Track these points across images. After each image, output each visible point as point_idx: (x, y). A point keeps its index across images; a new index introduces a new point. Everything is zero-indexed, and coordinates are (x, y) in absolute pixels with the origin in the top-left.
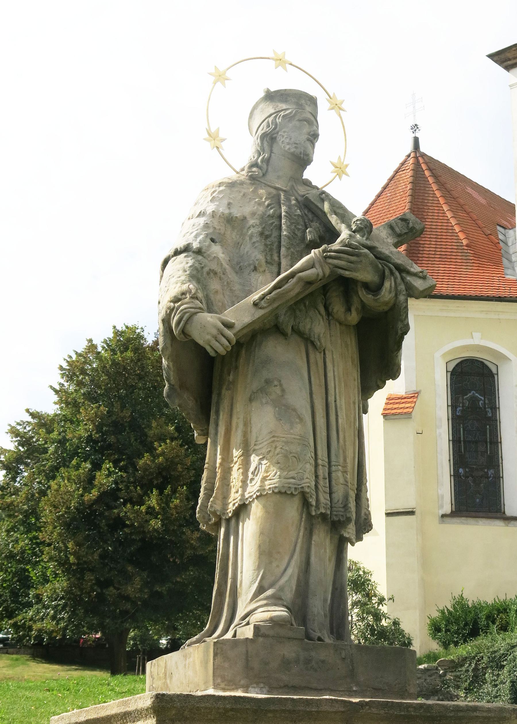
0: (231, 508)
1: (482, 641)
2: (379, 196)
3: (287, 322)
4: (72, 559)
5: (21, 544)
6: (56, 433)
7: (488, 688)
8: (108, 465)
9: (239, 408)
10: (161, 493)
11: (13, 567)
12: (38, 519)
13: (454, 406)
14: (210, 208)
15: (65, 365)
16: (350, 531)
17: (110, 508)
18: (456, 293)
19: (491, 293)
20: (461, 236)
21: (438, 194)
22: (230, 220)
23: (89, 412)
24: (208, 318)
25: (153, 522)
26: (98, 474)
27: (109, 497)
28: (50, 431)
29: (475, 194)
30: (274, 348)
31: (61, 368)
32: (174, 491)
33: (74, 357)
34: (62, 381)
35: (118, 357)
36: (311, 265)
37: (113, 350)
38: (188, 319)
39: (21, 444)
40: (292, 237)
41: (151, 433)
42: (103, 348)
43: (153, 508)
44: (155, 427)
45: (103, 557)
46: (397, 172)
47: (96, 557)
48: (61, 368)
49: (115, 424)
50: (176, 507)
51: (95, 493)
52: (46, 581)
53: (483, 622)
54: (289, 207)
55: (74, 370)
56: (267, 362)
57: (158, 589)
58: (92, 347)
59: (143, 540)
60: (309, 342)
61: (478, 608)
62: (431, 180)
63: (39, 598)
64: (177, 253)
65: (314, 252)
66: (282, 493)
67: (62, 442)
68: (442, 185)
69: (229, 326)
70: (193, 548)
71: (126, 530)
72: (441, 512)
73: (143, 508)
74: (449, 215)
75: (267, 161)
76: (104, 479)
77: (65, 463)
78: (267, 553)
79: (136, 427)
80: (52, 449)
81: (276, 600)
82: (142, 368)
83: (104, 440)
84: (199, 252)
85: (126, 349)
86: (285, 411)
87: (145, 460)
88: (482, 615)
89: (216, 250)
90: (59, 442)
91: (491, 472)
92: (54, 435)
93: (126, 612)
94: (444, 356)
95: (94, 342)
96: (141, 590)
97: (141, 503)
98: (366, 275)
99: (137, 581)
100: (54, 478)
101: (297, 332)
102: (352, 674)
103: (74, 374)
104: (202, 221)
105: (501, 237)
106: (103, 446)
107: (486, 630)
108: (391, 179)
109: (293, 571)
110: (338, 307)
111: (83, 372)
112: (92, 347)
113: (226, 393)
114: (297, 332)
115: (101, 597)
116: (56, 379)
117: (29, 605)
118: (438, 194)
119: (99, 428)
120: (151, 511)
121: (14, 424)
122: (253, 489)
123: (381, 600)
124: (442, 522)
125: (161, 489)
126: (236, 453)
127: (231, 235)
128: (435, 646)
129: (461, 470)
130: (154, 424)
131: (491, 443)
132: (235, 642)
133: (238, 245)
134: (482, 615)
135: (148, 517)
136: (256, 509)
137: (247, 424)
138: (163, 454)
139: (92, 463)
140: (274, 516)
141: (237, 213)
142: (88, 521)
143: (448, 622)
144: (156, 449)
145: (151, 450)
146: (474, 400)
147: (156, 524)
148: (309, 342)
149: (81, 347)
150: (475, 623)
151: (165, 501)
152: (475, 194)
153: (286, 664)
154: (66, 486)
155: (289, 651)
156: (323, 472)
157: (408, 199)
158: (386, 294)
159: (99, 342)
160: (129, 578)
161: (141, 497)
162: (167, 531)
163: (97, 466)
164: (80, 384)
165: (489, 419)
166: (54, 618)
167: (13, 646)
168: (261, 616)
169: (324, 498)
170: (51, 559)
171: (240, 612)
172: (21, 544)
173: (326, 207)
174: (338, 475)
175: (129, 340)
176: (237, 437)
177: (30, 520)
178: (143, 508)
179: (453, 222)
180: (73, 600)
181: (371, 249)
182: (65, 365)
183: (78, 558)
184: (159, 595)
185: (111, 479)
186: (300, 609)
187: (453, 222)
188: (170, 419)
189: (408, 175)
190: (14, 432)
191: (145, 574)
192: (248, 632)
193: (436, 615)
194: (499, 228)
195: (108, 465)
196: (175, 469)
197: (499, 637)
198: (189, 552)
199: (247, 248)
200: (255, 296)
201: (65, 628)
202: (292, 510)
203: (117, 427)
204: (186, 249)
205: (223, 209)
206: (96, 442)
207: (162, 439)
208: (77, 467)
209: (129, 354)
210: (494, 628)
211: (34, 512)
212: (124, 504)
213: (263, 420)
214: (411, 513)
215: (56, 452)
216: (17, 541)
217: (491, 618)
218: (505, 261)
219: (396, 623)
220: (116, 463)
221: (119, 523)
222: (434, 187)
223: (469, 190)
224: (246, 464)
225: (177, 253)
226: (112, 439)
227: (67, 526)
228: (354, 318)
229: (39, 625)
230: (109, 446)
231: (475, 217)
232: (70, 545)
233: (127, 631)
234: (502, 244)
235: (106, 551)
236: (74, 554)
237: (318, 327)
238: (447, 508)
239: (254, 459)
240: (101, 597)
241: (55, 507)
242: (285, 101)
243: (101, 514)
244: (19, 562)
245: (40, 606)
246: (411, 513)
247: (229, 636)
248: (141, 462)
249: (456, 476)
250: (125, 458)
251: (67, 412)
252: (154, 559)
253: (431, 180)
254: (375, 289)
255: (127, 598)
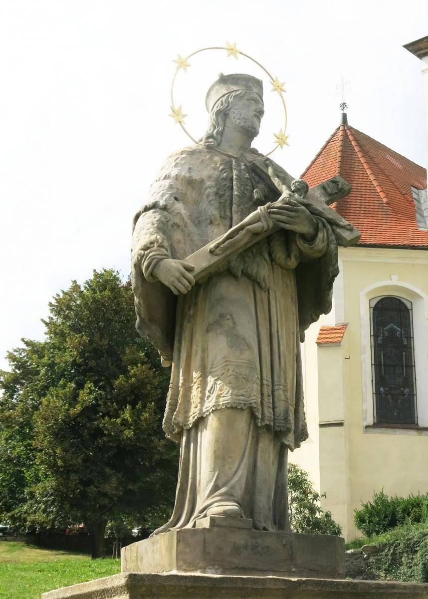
0: (191, 420)
1: (399, 530)
2: (314, 162)
3: (235, 264)
4: (60, 462)
5: (18, 450)
6: (46, 358)
7: (403, 569)
8: (89, 385)
9: (198, 337)
10: (133, 408)
11: (11, 469)
12: (31, 429)
13: (376, 335)
14: (174, 172)
15: (54, 302)
16: (290, 439)
17: (91, 420)
18: (377, 242)
19: (406, 243)
20: (382, 195)
21: (362, 160)
22: (190, 182)
23: (74, 340)
24: (173, 263)
25: (126, 432)
26: (81, 392)
27: (90, 411)
28: (41, 357)
29: (393, 161)
30: (231, 292)
31: (51, 305)
32: (144, 406)
33: (61, 295)
34: (51, 315)
35: (98, 295)
36: (257, 219)
37: (94, 290)
38: (155, 264)
39: (18, 367)
40: (242, 196)
41: (125, 358)
42: (86, 288)
43: (127, 420)
44: (128, 353)
45: (85, 460)
46: (328, 142)
47: (80, 461)
48: (51, 305)
49: (95, 351)
50: (146, 419)
51: (78, 408)
52: (38, 480)
53: (400, 515)
54: (240, 171)
55: (62, 306)
56: (221, 299)
57: (130, 487)
58: (76, 287)
59: (118, 447)
60: (256, 283)
61: (396, 503)
62: (357, 149)
63: (32, 495)
64: (146, 209)
65: (260, 209)
66: (233, 408)
67: (51, 366)
68: (365, 153)
69: (189, 269)
70: (160, 453)
71: (105, 439)
72: (365, 424)
73: (119, 421)
74: (372, 177)
75: (221, 133)
76: (87, 396)
77: (54, 383)
78: (221, 457)
79: (113, 353)
80: (43, 372)
81: (228, 496)
82: (118, 304)
83: (86, 364)
84: (165, 208)
85: (105, 289)
86: (236, 341)
87: (120, 381)
88: (399, 509)
89: (179, 207)
90: (49, 365)
91: (406, 391)
92: (45, 360)
93: (104, 506)
94: (367, 294)
95: (78, 283)
96: (117, 488)
97: (117, 416)
98: (303, 228)
99: (114, 481)
100: (44, 395)
101: (246, 275)
102: (291, 558)
103: (61, 309)
104: (167, 183)
105: (415, 196)
106: (82, 371)
107: (402, 521)
108: (324, 148)
109: (243, 472)
110: (280, 255)
111: (69, 308)
112: (76, 287)
113: (187, 325)
114: (246, 275)
115: (84, 495)
116: (47, 314)
117: (24, 501)
118: (362, 160)
119: (82, 354)
120: (125, 423)
121: (11, 351)
122: (209, 404)
123: (316, 497)
124: (366, 432)
125: (133, 404)
126: (196, 375)
127: (192, 195)
128: (360, 535)
129: (382, 389)
130: (127, 351)
131: (406, 366)
132: (194, 531)
133: (197, 203)
134: (399, 509)
135: (122, 428)
136: (212, 422)
137: (204, 350)
138: (135, 375)
139: (76, 383)
140: (227, 427)
141: (196, 176)
142: (70, 431)
143: (371, 515)
144: (129, 372)
145: (125, 372)
146: (392, 331)
147: (129, 433)
148: (256, 283)
149: (67, 287)
150: (394, 515)
151: (137, 415)
152: (393, 161)
153: (236, 549)
154: (54, 401)
155: (239, 538)
156: (267, 390)
157: (338, 165)
158: (320, 243)
159: (82, 283)
160: (107, 478)
161: (117, 411)
162: (138, 440)
163: (80, 386)
164: (66, 318)
165: (405, 346)
166: (44, 511)
167: (10, 534)
168: (216, 509)
169: (268, 412)
170: (42, 462)
171: (199, 507)
172: (18, 450)
173: (270, 171)
174: (280, 393)
175: (106, 281)
176: (196, 362)
177: (24, 430)
178: (119, 421)
179: (375, 183)
180: (61, 496)
181: (307, 206)
182: (54, 302)
183: (65, 462)
184: (132, 492)
185: (92, 397)
186: (248, 504)
187: (375, 183)
188: (141, 347)
189: (338, 144)
190: (11, 357)
191: (120, 475)
192: (205, 523)
193: (361, 508)
194: (413, 189)
195: (89, 385)
196: (145, 388)
197: (413, 527)
198: (156, 457)
199: (204, 205)
200: (212, 245)
201: (54, 520)
202: (242, 422)
203: (97, 353)
204: (154, 206)
205: (185, 173)
206: (79, 366)
207: (134, 363)
208: (64, 386)
209: (107, 293)
210: (409, 520)
211: (28, 424)
212: (103, 417)
213: (218, 347)
214: (340, 424)
215: (46, 374)
216: (14, 448)
217: (406, 512)
218: (418, 216)
219: (328, 516)
220: (96, 383)
221: (98, 433)
222: (360, 155)
223: (388, 157)
224: (204, 384)
225: (146, 209)
226: (93, 363)
227: (56, 435)
228: (293, 263)
229: (32, 517)
230: (91, 369)
231: (393, 179)
232: (58, 451)
233: (105, 522)
234: (415, 202)
235: (88, 456)
236: (62, 458)
237: (263, 271)
238: (370, 421)
239: (211, 380)
240: (84, 495)
241: (45, 419)
242: (236, 84)
243: (84, 425)
244: (16, 465)
245: (32, 501)
246: (340, 424)
247: (189, 526)
248: (117, 382)
249: (378, 394)
250: (104, 379)
251: (56, 341)
252: (127, 462)
253: (357, 149)
254: (310, 239)
255: (105, 495)
